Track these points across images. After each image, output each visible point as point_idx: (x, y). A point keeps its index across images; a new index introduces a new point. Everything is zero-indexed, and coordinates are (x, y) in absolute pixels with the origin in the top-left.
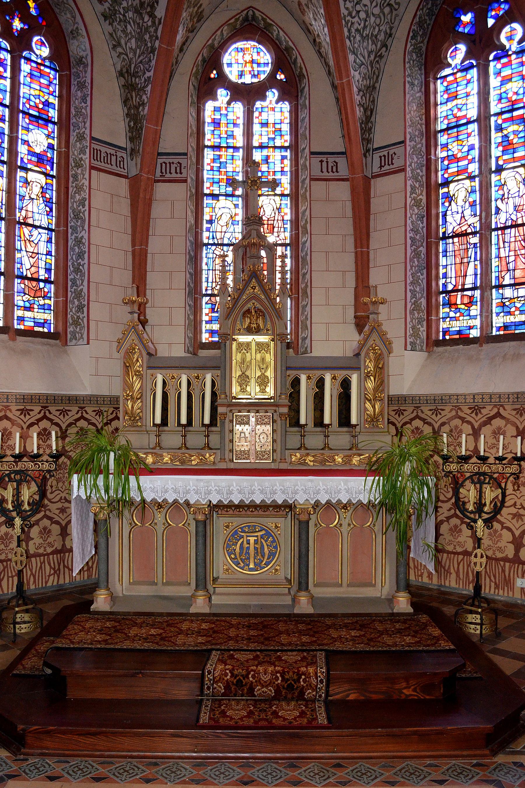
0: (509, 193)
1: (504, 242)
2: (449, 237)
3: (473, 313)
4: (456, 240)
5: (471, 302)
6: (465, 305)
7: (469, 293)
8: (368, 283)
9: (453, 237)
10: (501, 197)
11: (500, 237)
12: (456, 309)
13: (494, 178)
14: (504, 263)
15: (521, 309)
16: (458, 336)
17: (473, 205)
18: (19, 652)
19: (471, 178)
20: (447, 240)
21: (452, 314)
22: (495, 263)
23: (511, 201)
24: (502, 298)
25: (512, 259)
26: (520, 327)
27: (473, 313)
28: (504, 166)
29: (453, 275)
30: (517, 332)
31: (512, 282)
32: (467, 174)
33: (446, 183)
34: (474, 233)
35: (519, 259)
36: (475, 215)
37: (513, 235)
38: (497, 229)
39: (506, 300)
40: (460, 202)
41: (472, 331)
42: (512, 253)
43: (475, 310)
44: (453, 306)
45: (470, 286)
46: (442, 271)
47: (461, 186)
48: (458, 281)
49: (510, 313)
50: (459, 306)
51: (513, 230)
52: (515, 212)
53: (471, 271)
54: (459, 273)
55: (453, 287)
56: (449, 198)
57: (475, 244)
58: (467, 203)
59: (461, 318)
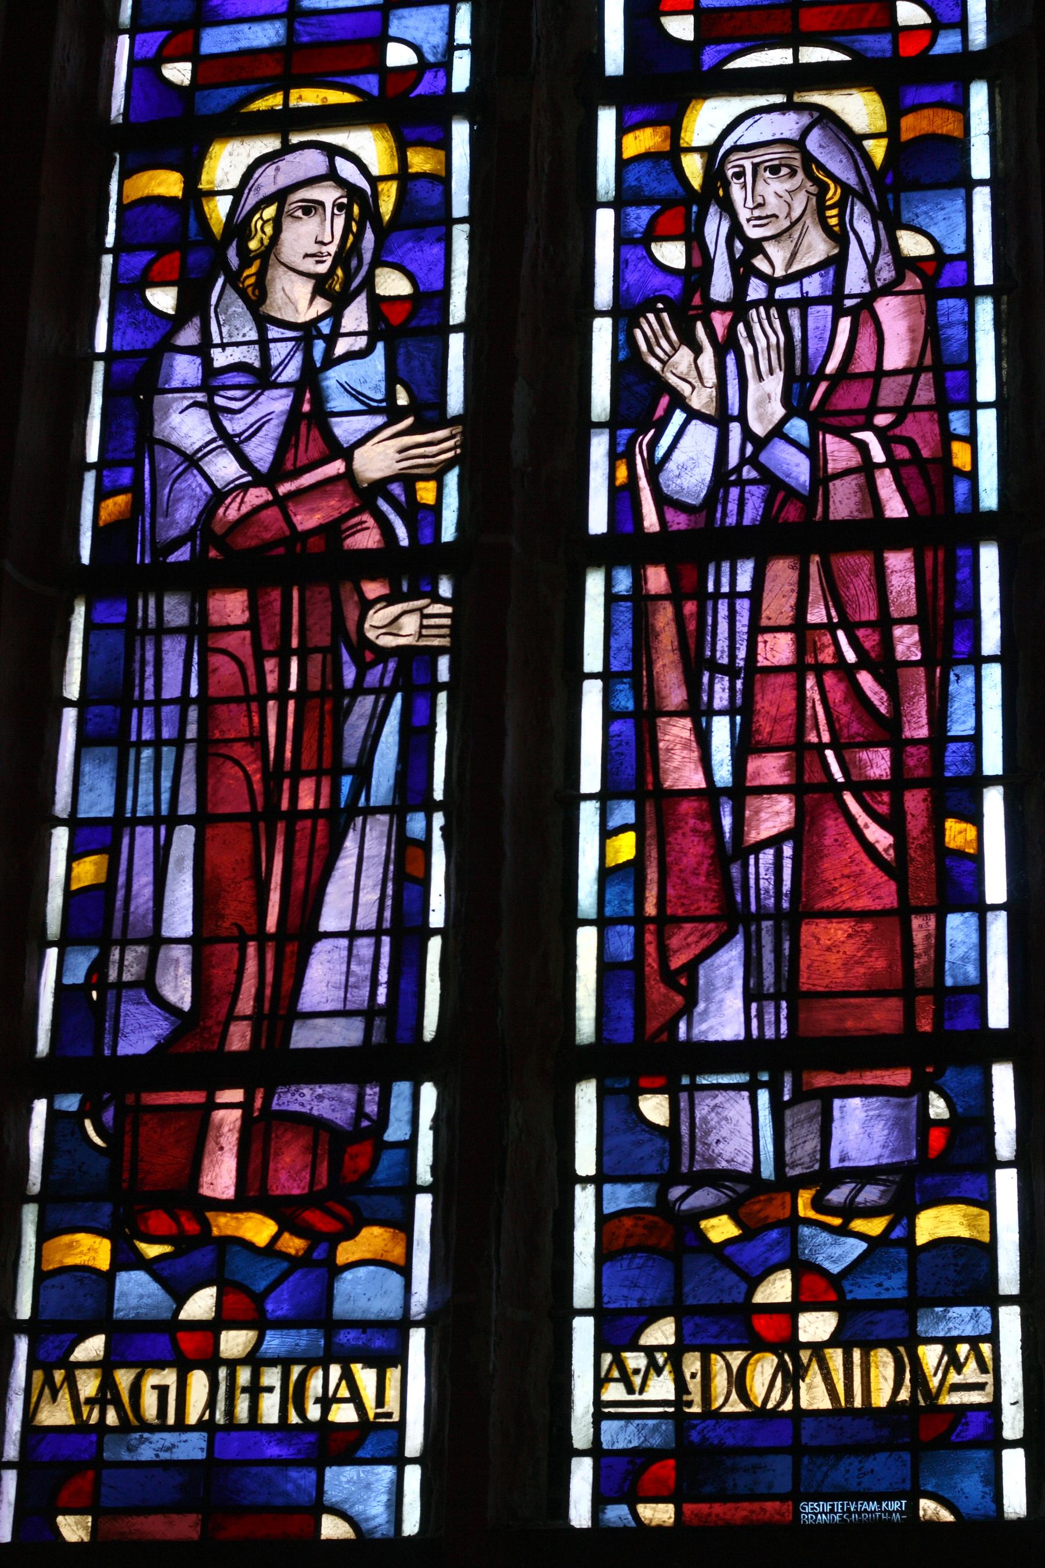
0: (742, 271)
1: (696, 664)
2: (164, 579)
3: (362, 1293)
4: (231, 607)
5: (354, 1184)
6: (285, 1213)
7: (327, 1102)
8: (471, 129)
9: (199, 582)
10: (675, 289)
11: (664, 617)
12: (183, 1244)
13: (611, 142)
14: (691, 850)
15: (862, 1291)
16: (184, 1527)
17: (408, 332)
18: (967, 1236)
19: (410, 110)
20: (147, 608)
21: (136, 1292)
22: (598, 845)
23: (763, 336)
24: (665, 1180)
25: (775, 816)
26: (846, 1471)
27: (362, 1293)
28: (709, 57)
29: (179, 919)
30: (816, 1512)
31: (776, 1024)
32: (371, 83)
33: (179, 132)
34: (408, 571)
35: (833, 826)
36: (428, 413)
37: (778, 605)
38: (625, 545)
39: (704, 1197)
40: (295, 299)
41: (341, 1481)
42: (769, 768)
43: (390, 1271)
44: (158, 1220)
45: (346, 1034)
46: (63, 868)
47: (313, 162)
48: (221, 977)
49: (728, 1324)
50: (223, 1224)
51: (782, 573)
52: (798, 428)
53: (352, 891)
54: (235, 909)
55: (161, 1027)
56: (210, 257)
57: (414, 661)
58: (356, 316)
59: (234, 1342)
